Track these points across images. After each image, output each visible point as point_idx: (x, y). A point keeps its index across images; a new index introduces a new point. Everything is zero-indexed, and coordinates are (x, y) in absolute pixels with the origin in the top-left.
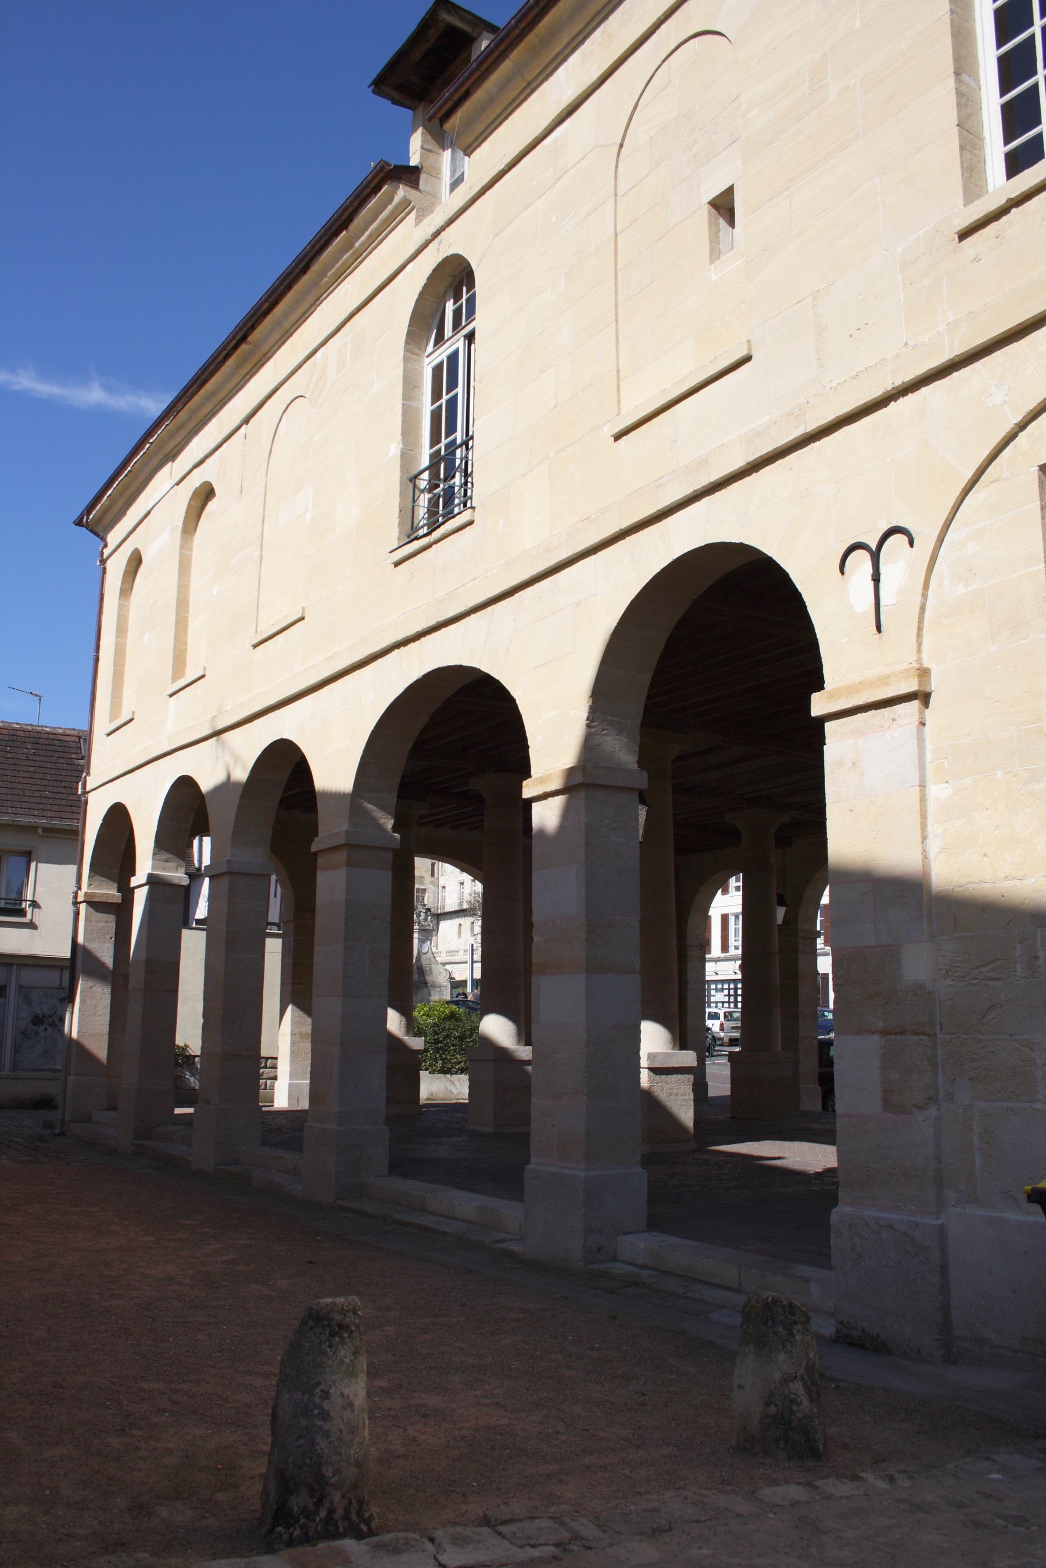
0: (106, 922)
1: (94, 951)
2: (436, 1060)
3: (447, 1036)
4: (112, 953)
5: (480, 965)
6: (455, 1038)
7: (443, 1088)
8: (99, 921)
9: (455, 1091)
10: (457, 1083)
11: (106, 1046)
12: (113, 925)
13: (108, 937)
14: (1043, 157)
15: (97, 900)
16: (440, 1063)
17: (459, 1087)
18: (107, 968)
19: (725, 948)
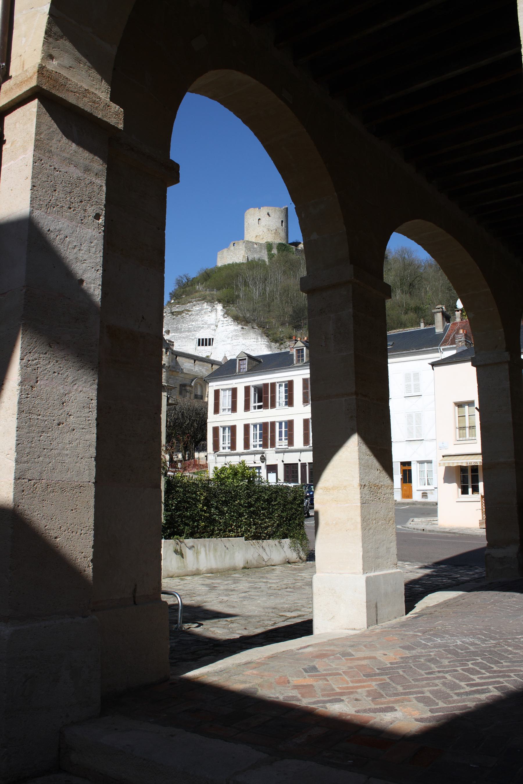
0: (87, 170)
1: (57, 242)
2: (250, 525)
3: (258, 500)
4: (99, 259)
5: (162, 444)
6: (264, 501)
7: (256, 555)
8: (70, 161)
9: (266, 558)
10: (267, 549)
11: (88, 518)
12: (101, 182)
13: (91, 211)
14: (178, 166)
15: (71, 99)
16: (253, 529)
17: (268, 553)
18: (87, 296)
19: (247, 445)
